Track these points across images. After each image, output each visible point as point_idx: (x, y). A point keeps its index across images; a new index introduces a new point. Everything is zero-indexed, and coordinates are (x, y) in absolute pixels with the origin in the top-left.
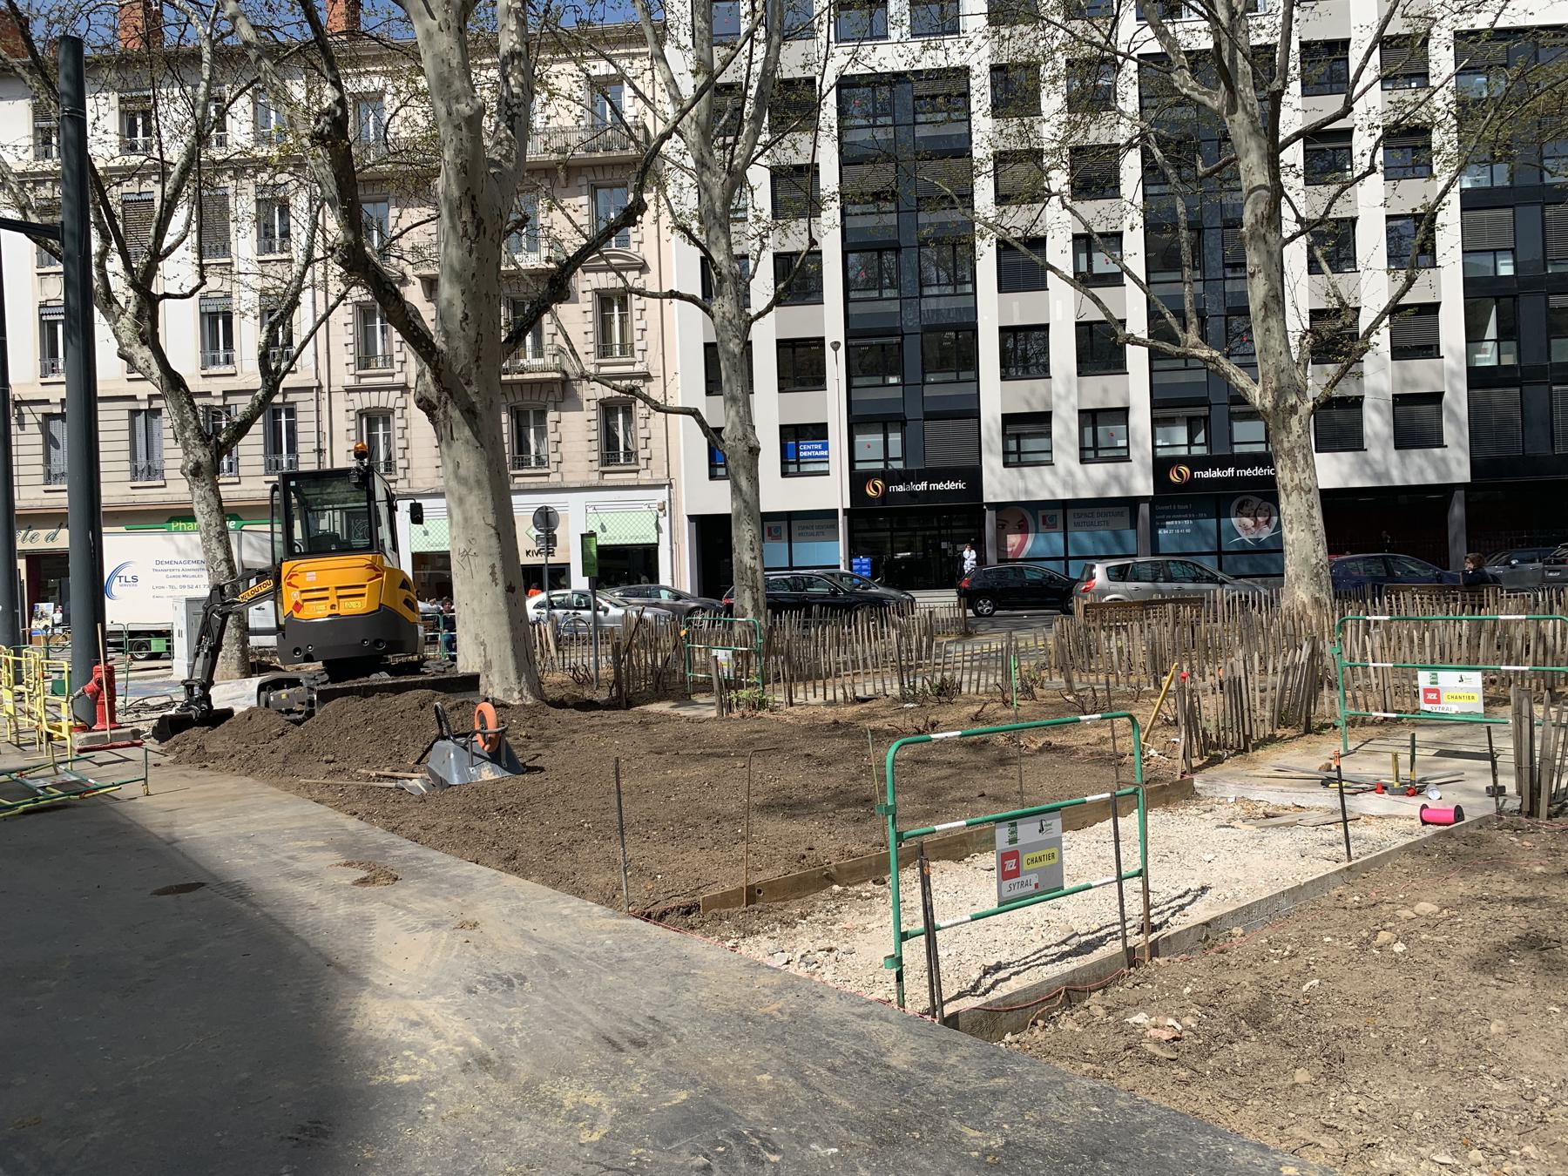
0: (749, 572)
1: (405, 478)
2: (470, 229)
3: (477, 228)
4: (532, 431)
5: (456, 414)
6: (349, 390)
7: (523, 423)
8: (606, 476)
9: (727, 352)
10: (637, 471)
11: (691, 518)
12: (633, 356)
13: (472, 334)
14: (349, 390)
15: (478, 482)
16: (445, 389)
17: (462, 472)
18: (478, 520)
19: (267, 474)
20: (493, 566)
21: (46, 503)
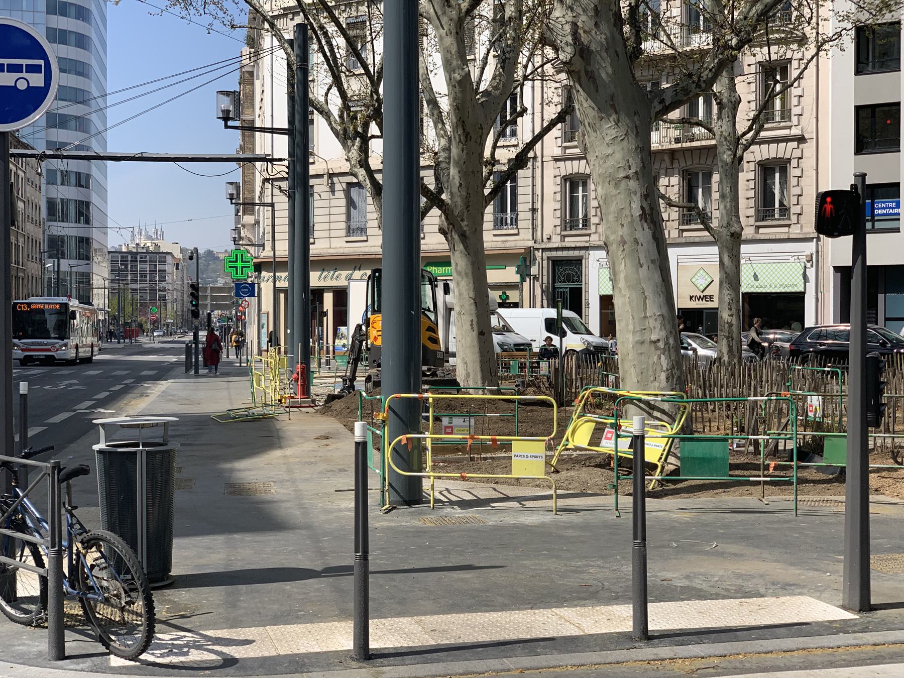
0: (726, 326)
1: (596, 232)
2: (462, 138)
3: (466, 137)
4: (700, 190)
5: (456, 237)
6: (557, 160)
7: (694, 184)
8: (761, 230)
9: (722, 161)
10: (789, 226)
11: (837, 269)
12: (790, 121)
13: (464, 194)
14: (557, 160)
15: (466, 274)
16: (451, 224)
17: (459, 268)
18: (465, 295)
19: (495, 229)
20: (472, 321)
21: (347, 251)
